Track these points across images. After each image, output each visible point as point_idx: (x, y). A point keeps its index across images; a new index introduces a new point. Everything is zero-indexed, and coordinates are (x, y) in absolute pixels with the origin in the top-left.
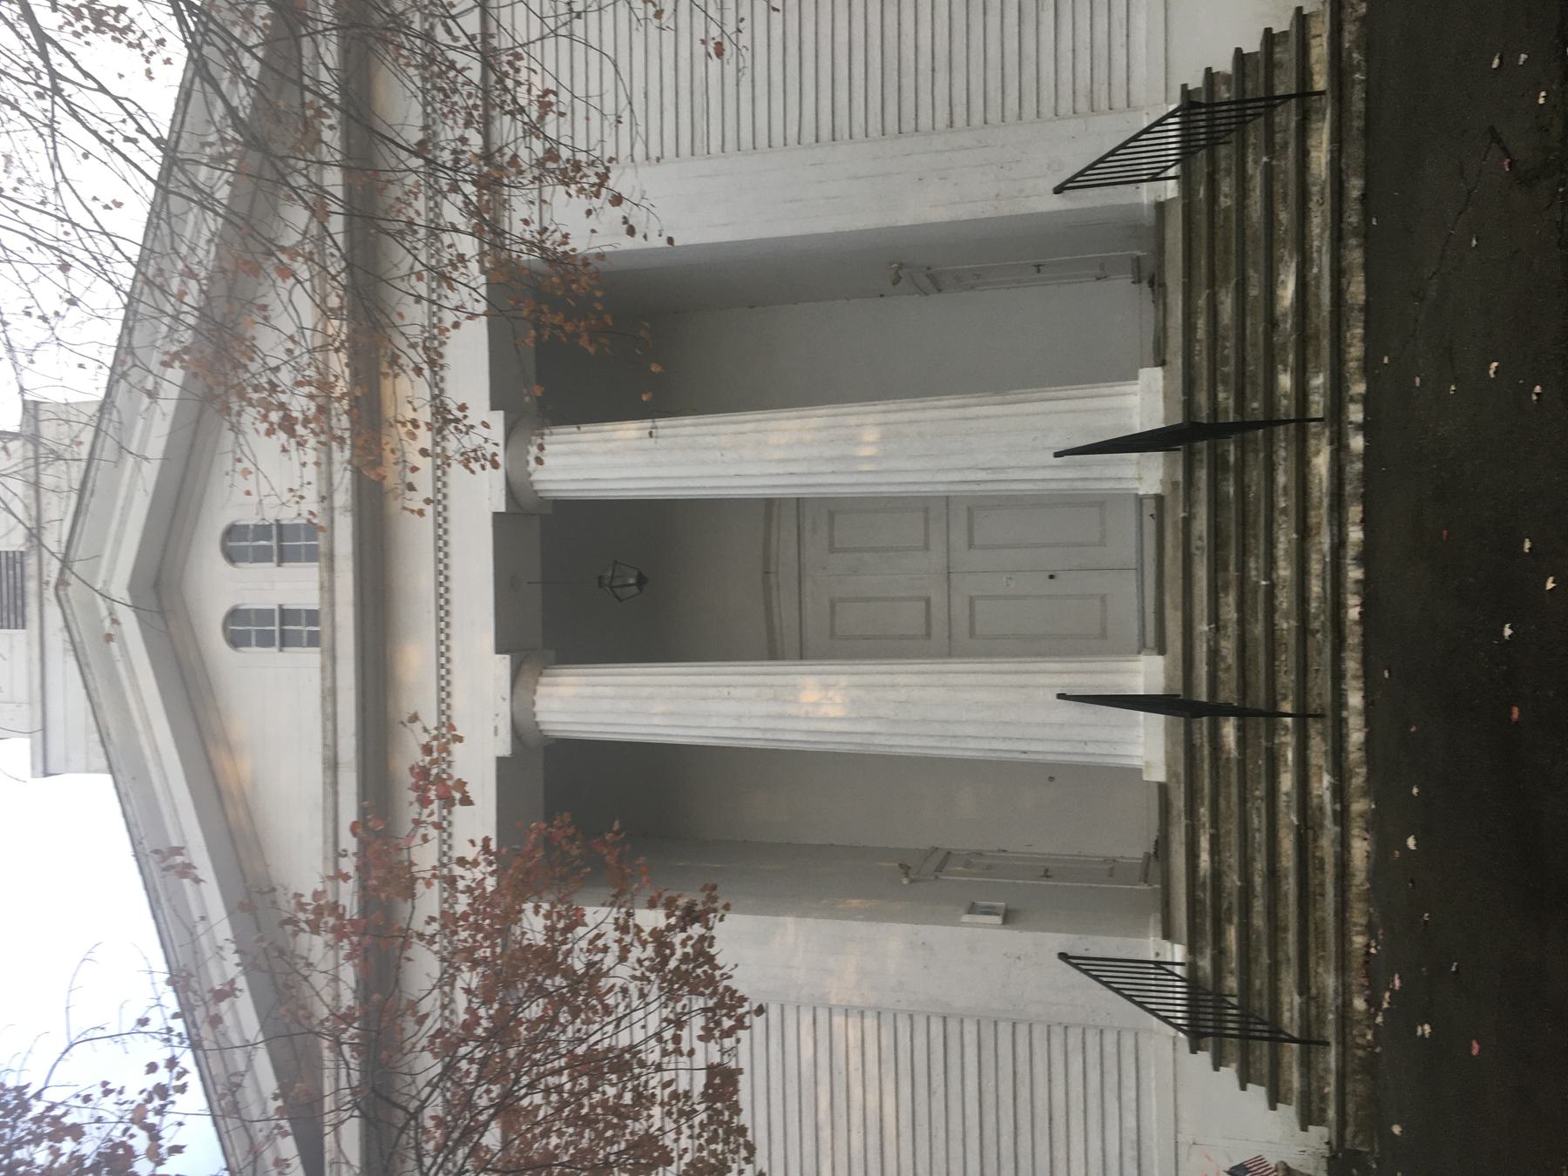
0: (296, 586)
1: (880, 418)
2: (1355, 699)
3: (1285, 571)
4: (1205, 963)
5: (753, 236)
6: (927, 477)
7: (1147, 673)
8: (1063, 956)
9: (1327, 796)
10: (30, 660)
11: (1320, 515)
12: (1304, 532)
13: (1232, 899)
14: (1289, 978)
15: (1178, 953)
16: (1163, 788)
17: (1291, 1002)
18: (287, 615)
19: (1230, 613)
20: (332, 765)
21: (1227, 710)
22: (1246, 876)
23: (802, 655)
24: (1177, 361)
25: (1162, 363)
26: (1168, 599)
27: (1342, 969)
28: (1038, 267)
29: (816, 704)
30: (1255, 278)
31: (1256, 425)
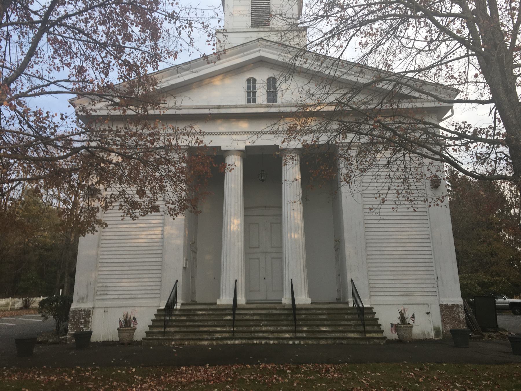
0: (261, 97)
1: (300, 238)
2: (237, 342)
3: (264, 329)
4: (177, 313)
5: (343, 208)
6: (287, 250)
7: (241, 300)
8: (177, 281)
9: (217, 336)
10: (243, 29)
11: (276, 335)
12: (272, 332)
13: (192, 318)
14: (177, 329)
15: (178, 307)
16: (215, 304)
17: (172, 330)
18: (254, 93)
19: (255, 318)
20: (219, 107)
21: (234, 317)
22: (197, 321)
23: (245, 216)
24: (312, 307)
25: (312, 303)
26: (258, 305)
27: (180, 339)
28: (339, 275)
29: (234, 223)
30: (329, 323)
31: (295, 323)
